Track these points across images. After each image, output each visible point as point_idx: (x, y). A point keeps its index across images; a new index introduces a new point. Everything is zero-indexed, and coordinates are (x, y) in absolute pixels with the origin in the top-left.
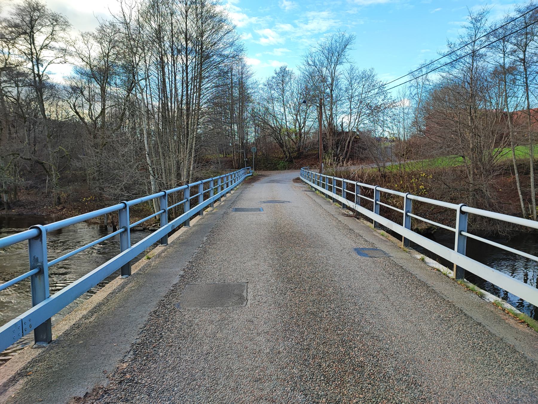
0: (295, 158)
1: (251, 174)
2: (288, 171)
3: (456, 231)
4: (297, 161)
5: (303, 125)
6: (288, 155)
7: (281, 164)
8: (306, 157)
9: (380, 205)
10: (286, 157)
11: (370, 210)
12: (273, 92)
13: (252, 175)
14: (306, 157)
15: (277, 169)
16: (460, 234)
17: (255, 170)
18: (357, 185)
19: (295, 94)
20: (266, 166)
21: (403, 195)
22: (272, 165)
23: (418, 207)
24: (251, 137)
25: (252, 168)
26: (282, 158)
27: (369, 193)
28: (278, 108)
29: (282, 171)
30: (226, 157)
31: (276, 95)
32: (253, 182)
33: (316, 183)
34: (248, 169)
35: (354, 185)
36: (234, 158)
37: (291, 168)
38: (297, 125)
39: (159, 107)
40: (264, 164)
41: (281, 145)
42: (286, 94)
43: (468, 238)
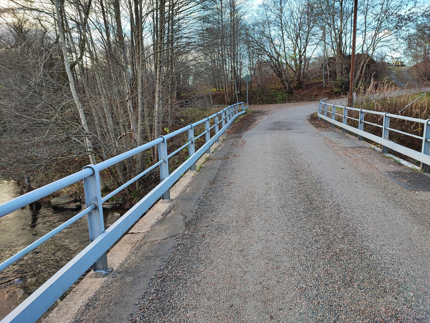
0: (295, 88)
1: (244, 112)
2: (290, 104)
3: (423, 138)
4: (297, 92)
5: (303, 50)
6: (287, 86)
7: (279, 96)
8: (308, 87)
9: (364, 123)
10: (285, 88)
11: (417, 150)
12: (269, 13)
13: (246, 113)
14: (308, 87)
15: (275, 102)
16: (385, 128)
17: (250, 104)
18: (361, 112)
19: (295, 14)
20: (261, 99)
21: (383, 114)
22: (269, 98)
23: (393, 122)
24: (245, 72)
25: (245, 102)
26: (280, 89)
27: (378, 120)
28: (274, 32)
29: (283, 105)
30: (219, 90)
31: (273, 17)
32: (247, 129)
33: (326, 113)
34: (241, 104)
35: (358, 112)
36: (226, 92)
37: (291, 100)
38: (297, 51)
39: (132, 40)
40: (260, 96)
41: (280, 75)
42: (285, 14)
43: (390, 131)
